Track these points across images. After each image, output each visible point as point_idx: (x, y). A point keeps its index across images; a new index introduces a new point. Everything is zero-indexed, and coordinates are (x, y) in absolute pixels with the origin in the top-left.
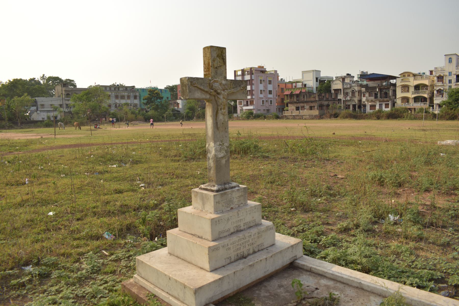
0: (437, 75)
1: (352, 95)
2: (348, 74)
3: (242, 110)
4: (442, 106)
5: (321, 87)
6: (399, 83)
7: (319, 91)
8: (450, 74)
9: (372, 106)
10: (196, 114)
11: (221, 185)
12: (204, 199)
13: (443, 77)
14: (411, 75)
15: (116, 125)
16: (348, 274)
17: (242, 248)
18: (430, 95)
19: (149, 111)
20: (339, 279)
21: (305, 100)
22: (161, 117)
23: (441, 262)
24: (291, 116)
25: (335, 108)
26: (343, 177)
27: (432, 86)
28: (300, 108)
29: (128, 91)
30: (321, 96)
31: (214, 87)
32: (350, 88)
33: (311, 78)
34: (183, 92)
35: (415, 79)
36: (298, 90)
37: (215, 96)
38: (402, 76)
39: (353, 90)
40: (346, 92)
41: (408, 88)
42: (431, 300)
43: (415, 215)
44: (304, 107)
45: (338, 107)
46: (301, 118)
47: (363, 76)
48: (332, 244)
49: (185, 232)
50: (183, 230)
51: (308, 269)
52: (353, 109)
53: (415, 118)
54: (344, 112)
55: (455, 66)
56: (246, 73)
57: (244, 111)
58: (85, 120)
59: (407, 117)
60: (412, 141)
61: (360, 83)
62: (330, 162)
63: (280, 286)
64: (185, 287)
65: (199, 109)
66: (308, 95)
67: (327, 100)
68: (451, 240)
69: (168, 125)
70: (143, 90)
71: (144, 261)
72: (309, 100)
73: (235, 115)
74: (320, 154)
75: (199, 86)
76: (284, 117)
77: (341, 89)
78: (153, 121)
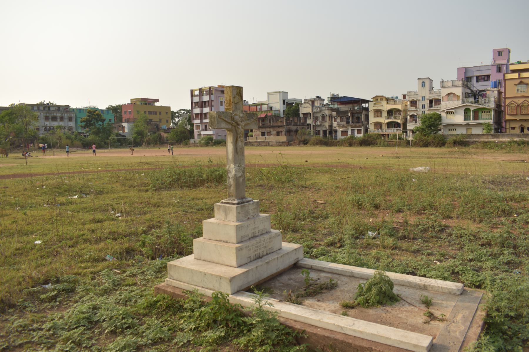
0: (411, 100)
1: (322, 120)
2: (318, 97)
3: (200, 135)
4: (416, 132)
5: (289, 111)
6: (371, 107)
7: (287, 115)
8: (423, 98)
9: (344, 132)
10: (145, 140)
11: (239, 199)
12: (226, 212)
13: (416, 102)
14: (384, 99)
15: (48, 152)
16: (342, 268)
17: (259, 249)
18: (403, 120)
19: (88, 136)
20: (335, 272)
21: (272, 125)
22: (103, 143)
23: (412, 262)
24: (256, 142)
25: (305, 134)
26: (323, 202)
27: (406, 111)
28: (266, 134)
29: (61, 111)
30: (289, 120)
31: (235, 119)
32: (321, 111)
33: (278, 101)
34: (211, 123)
35: (388, 104)
36: (263, 113)
37: (235, 127)
38: (375, 100)
39: (324, 115)
40: (316, 116)
41: (381, 113)
42: (404, 278)
43: (391, 230)
44: (270, 132)
45: (307, 133)
46: (267, 144)
47: (334, 99)
48: (322, 254)
49: (210, 239)
50: (207, 238)
51: (310, 267)
52: (323, 135)
53: (389, 145)
54: (314, 138)
55: (428, 90)
56: (205, 92)
57: (202, 136)
58: (8, 146)
59: (380, 144)
60: (386, 168)
61: (331, 106)
62: (307, 189)
63: (290, 279)
64: (221, 278)
65: (149, 134)
66: (274, 119)
67: (296, 125)
68: (420, 248)
69: (113, 152)
70: (80, 110)
71: (176, 265)
72: (275, 124)
73: (192, 141)
74: (296, 182)
75: (224, 118)
76: (249, 143)
77: (310, 113)
78: (96, 148)
